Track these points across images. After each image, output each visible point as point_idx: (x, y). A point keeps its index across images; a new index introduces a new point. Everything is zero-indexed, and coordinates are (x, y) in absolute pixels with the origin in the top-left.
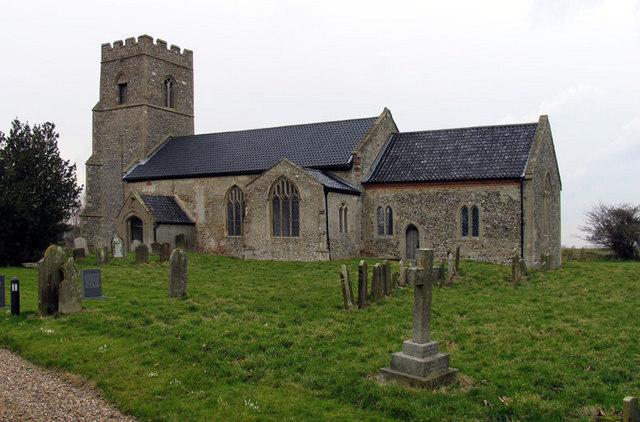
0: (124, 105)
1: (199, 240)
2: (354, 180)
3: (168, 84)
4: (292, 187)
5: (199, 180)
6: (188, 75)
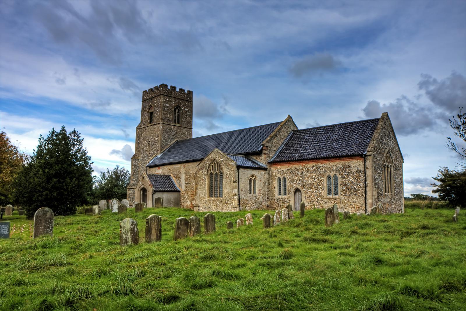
0: (152, 124)
1: (182, 201)
2: (262, 161)
3: (177, 111)
4: (220, 166)
5: (183, 165)
6: (189, 105)
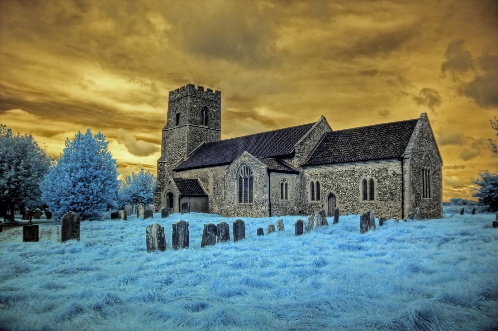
0: (178, 126)
1: (210, 206)
2: (295, 163)
3: (204, 112)
5: (211, 169)
6: (217, 106)
